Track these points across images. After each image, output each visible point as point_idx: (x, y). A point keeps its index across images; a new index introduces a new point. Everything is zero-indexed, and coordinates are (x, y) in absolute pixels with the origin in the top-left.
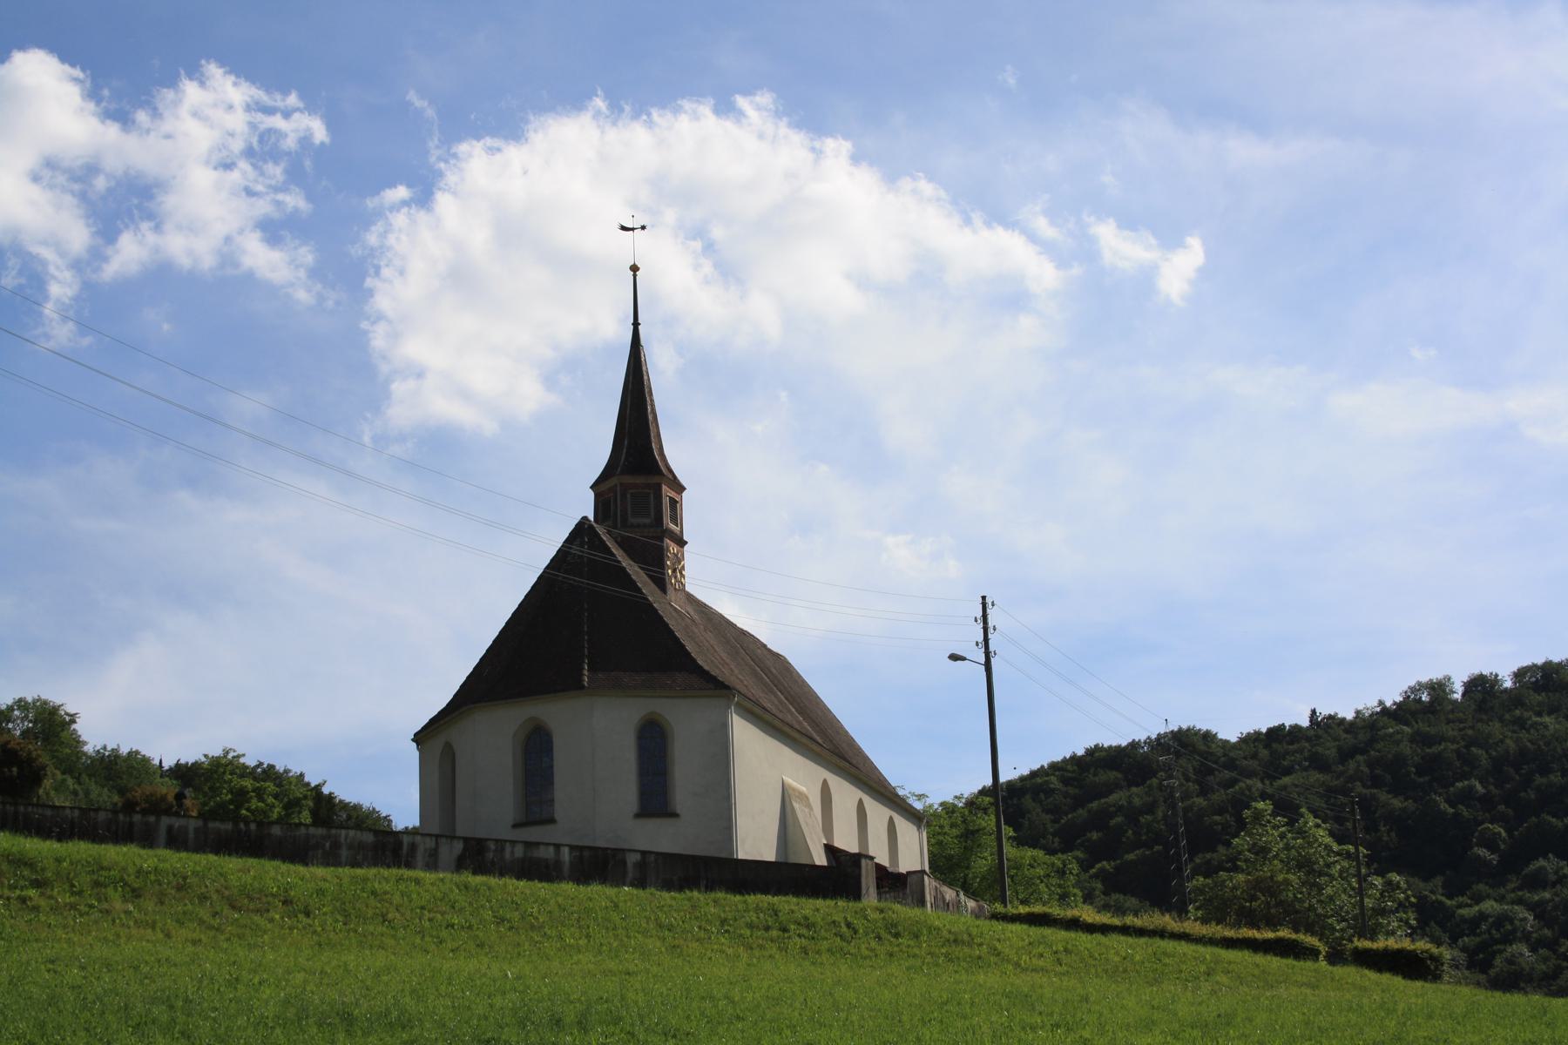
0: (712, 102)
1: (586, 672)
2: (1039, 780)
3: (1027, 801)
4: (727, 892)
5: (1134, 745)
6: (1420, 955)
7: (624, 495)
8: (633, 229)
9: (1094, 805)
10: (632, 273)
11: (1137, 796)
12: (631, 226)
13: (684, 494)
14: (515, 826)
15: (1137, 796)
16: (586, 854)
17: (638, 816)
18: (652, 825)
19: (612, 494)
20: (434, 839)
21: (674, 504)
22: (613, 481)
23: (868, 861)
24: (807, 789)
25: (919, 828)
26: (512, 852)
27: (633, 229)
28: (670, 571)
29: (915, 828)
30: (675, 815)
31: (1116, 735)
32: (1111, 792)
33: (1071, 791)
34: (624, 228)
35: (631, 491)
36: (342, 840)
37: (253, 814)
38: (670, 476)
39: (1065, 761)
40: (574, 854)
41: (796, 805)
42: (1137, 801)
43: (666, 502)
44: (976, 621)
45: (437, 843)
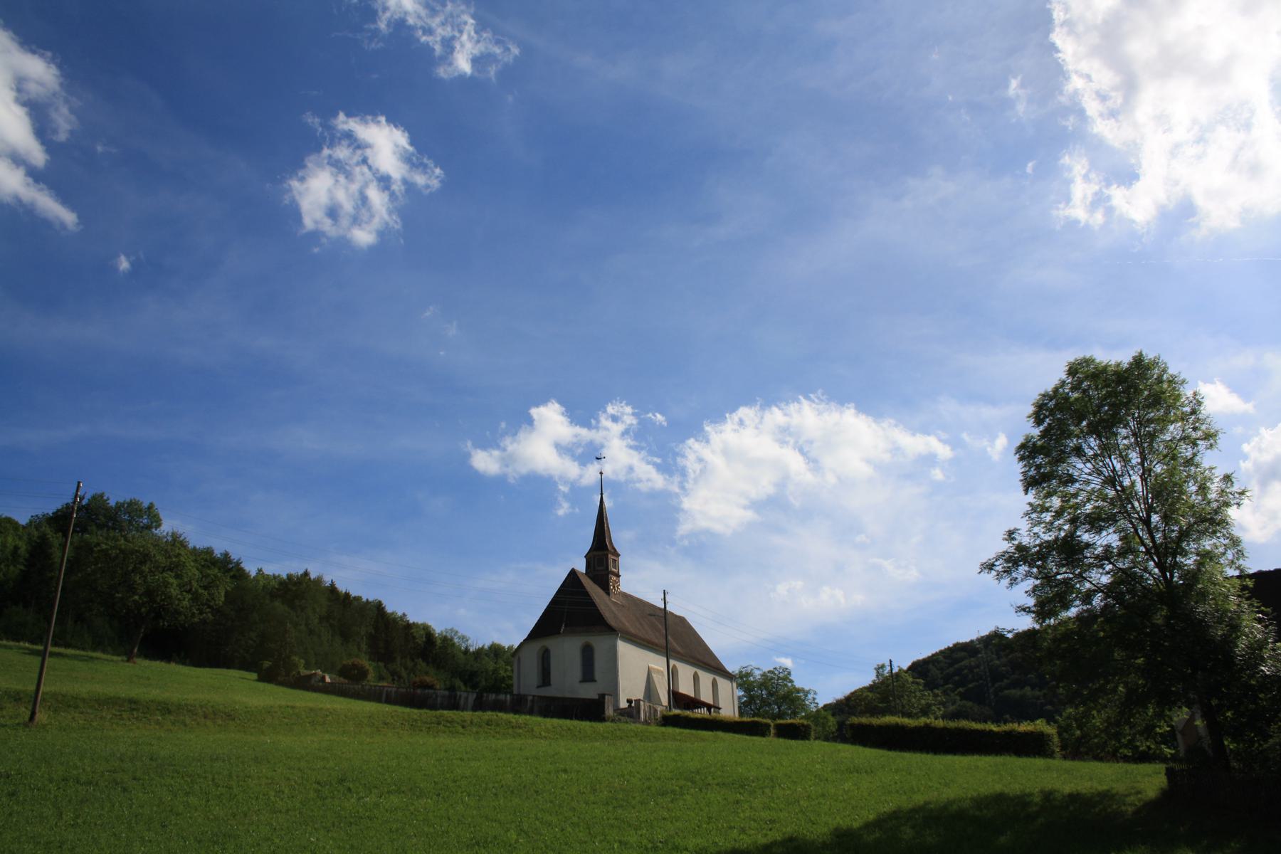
2: (934, 657)
3: (931, 666)
5: (972, 641)
9: (956, 666)
11: (973, 661)
14: (538, 687)
15: (973, 661)
16: (536, 698)
17: (580, 682)
18: (587, 685)
21: (614, 561)
23: (610, 697)
25: (731, 682)
30: (595, 681)
31: (965, 638)
32: (963, 660)
33: (947, 661)
38: (613, 551)
39: (945, 649)
42: (973, 663)
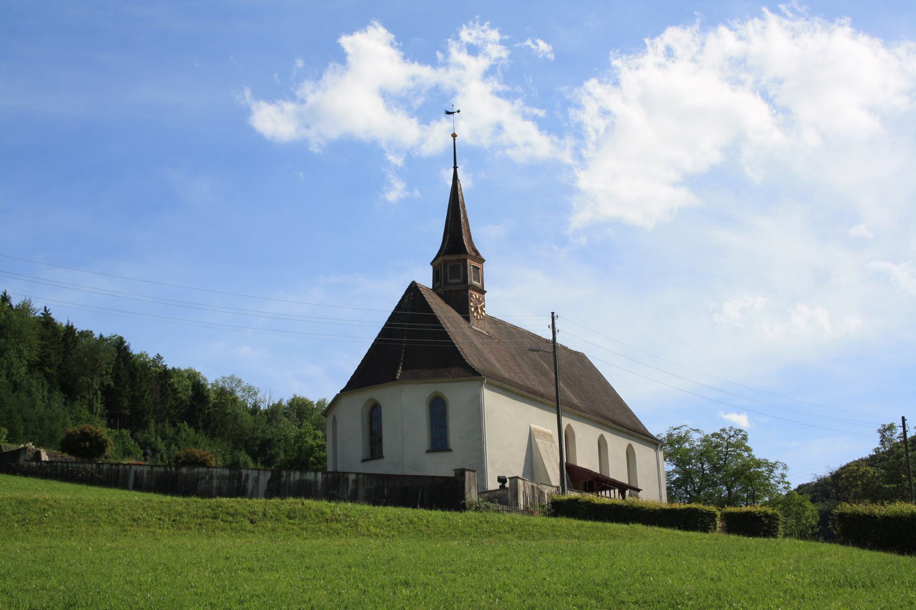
0: (849, 19)
1: (400, 371)
4: (172, 496)
6: (758, 515)
7: (445, 267)
13: (484, 264)
14: (363, 461)
20: (257, 471)
22: (440, 259)
25: (656, 450)
26: (294, 477)
28: (473, 309)
29: (652, 450)
30: (450, 450)
35: (449, 264)
36: (214, 474)
40: (323, 476)
41: (537, 440)
43: (470, 270)
44: (549, 327)
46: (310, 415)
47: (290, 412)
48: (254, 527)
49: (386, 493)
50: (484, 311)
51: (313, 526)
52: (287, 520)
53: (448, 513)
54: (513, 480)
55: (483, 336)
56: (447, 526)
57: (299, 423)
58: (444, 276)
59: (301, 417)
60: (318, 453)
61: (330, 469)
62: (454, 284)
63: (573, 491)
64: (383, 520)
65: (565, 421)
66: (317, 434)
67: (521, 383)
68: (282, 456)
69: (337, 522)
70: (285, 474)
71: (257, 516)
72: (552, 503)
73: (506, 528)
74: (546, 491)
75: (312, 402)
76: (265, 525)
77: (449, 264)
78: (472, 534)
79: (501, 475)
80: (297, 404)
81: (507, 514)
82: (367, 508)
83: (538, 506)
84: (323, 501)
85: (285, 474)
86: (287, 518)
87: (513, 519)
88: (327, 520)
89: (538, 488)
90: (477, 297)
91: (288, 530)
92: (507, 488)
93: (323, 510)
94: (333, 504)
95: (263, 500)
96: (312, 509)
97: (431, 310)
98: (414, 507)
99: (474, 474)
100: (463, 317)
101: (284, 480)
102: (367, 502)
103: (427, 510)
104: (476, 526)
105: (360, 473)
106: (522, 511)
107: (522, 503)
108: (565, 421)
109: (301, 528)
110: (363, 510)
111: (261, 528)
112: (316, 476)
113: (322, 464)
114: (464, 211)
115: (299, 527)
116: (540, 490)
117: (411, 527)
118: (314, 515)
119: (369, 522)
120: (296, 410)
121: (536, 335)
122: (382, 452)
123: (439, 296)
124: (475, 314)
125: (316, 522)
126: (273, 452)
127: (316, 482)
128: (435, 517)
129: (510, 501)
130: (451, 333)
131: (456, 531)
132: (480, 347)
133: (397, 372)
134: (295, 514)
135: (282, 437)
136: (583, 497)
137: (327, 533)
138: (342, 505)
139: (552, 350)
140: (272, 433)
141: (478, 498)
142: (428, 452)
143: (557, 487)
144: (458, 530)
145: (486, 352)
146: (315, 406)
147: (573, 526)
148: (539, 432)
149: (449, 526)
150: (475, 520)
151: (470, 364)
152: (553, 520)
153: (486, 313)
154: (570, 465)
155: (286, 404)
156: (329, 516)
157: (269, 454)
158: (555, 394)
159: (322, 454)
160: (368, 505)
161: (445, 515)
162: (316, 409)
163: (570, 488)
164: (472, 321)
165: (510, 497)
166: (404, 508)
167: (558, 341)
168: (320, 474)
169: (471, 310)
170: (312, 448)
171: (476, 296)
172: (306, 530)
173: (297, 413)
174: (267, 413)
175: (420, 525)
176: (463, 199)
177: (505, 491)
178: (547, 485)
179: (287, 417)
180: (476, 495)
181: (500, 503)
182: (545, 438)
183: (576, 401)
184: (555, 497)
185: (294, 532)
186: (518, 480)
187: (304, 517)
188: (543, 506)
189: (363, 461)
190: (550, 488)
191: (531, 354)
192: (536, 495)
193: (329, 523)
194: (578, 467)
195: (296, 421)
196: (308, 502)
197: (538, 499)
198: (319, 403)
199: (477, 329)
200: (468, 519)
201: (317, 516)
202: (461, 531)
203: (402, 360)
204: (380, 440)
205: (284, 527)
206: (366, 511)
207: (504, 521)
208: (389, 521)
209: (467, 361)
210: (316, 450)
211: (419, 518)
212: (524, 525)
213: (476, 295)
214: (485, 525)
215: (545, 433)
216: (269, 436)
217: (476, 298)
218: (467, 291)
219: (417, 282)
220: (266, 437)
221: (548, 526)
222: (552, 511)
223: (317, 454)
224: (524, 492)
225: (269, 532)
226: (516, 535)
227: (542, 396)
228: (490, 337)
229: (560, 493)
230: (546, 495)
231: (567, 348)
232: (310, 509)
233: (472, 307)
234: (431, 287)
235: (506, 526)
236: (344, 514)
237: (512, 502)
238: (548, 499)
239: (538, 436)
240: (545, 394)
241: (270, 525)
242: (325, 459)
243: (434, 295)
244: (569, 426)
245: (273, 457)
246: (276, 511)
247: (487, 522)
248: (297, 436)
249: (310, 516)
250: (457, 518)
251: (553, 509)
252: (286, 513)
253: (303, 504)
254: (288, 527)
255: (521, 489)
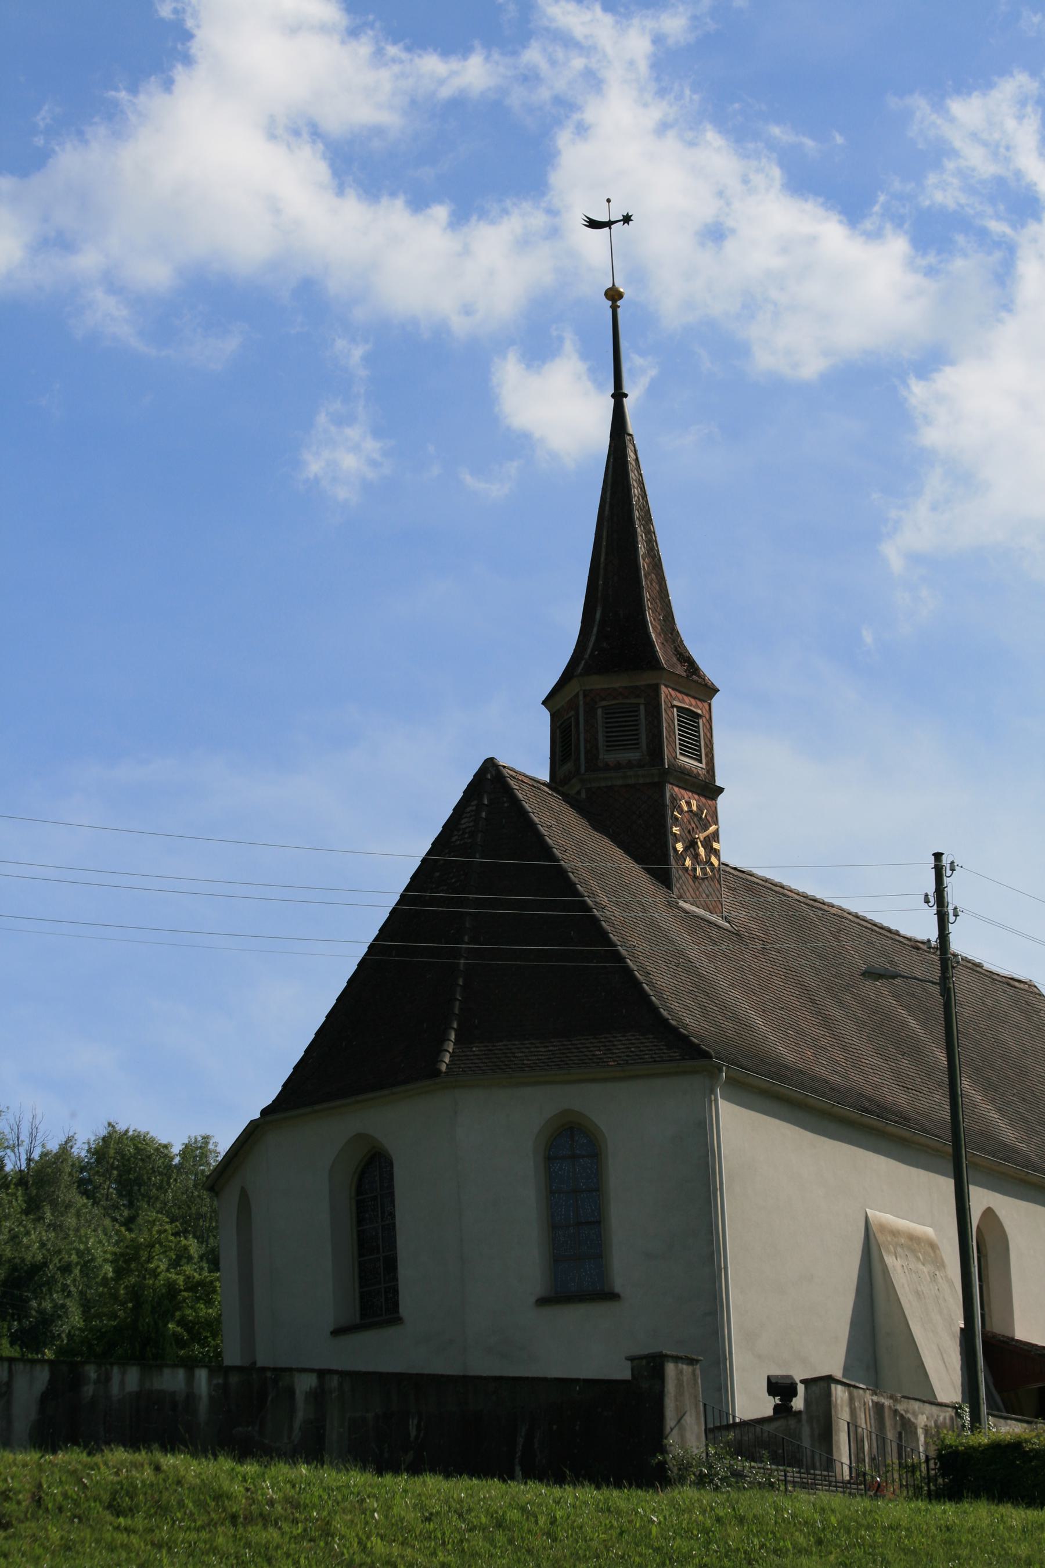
8: (609, 224)
10: (610, 303)
12: (604, 219)
13: (716, 701)
19: (572, 713)
20: (6, 1365)
23: (686, 1368)
24: (935, 1231)
26: (122, 1383)
27: (609, 224)
28: (680, 847)
30: (613, 1296)
34: (593, 224)
35: (604, 703)
37: (189, 1331)
40: (215, 1382)
41: (890, 1260)
43: (670, 719)
44: (927, 901)
45: (10, 1371)
46: (160, 1188)
47: (98, 1180)
48: (6, 1538)
49: (413, 1433)
50: (717, 853)
51: (193, 1536)
52: (109, 1517)
53: (616, 1493)
54: (815, 1389)
55: (714, 933)
56: (614, 1533)
57: (126, 1213)
58: (586, 740)
59: (130, 1194)
60: (192, 1308)
61: (232, 1357)
62: (618, 766)
63: (1006, 1418)
64: (412, 1516)
65: (980, 1199)
66: (186, 1248)
67: (836, 1079)
68: (75, 1318)
69: (265, 1527)
70: (93, 1375)
71: (14, 1507)
72: (940, 1457)
73: (801, 1540)
74: (921, 1421)
75: (166, 1146)
76: (42, 1534)
77: (604, 703)
78: (694, 1557)
79: (777, 1371)
80: (120, 1152)
81: (803, 1495)
82: (358, 1479)
83: (896, 1467)
84: (221, 1459)
85: (93, 1375)
86: (107, 1512)
87: (823, 1510)
88: (234, 1518)
89: (896, 1411)
90: (694, 808)
91: (111, 1548)
92: (800, 1412)
93: (220, 1487)
94: (250, 1468)
95: (32, 1457)
96: (186, 1486)
97: (547, 852)
98: (506, 1475)
99: (694, 1373)
100: (648, 871)
101: (91, 1393)
102: (360, 1464)
103: (548, 1485)
104: (706, 1531)
105: (330, 1372)
106: (846, 1484)
107: (846, 1460)
108: (980, 1199)
109: (153, 1544)
110: (348, 1486)
111: (28, 1540)
112: (190, 1379)
113: (204, 1343)
114: (650, 533)
115: (148, 1538)
116: (902, 1416)
117: (500, 1537)
118: (194, 1502)
119: (367, 1523)
120: (115, 1172)
121: (882, 928)
122: (396, 1305)
123: (572, 806)
124: (688, 863)
125: (199, 1523)
126: (47, 1305)
127: (191, 1397)
128: (574, 1506)
129: (809, 1453)
130: (613, 925)
131: (642, 1549)
132: (705, 965)
133: (440, 1050)
134: (131, 1498)
135: (74, 1258)
136: (1038, 1436)
137: (237, 1558)
138: (282, 1470)
139: (936, 975)
140: (43, 1245)
141: (707, 1445)
142: (543, 1302)
143: (956, 1408)
144: (650, 1546)
145: (724, 984)
146: (177, 1160)
147: (1012, 1527)
148: (895, 1233)
149: (621, 1533)
150: (703, 1512)
151: (673, 1023)
152: (947, 1511)
153: (723, 859)
154: (995, 1336)
155: (83, 1154)
156: (237, 1507)
157: (34, 1313)
158: (947, 1116)
159: (204, 1311)
160: (364, 1469)
161: (606, 1501)
162: (179, 1167)
163: (994, 1410)
164: (676, 886)
165: (806, 1443)
166: (475, 1481)
167: (958, 945)
168: (202, 1375)
169: (675, 849)
170: (172, 1289)
171: (689, 804)
172: (169, 1549)
173: (118, 1181)
174: (26, 1183)
175: (529, 1531)
176: (644, 495)
177: (792, 1422)
178: (924, 1402)
179: (86, 1193)
180: (698, 1438)
181: (776, 1460)
182: (913, 1251)
183: (1009, 1134)
184: (950, 1439)
185: (133, 1555)
186: (833, 1386)
187: (162, 1509)
188: (913, 1468)
189: (336, 1332)
190: (934, 1409)
191: (870, 989)
192: (890, 1435)
193: (241, 1530)
194: (1018, 1341)
195: (116, 1207)
196: (170, 1461)
197: (895, 1446)
198: (188, 1151)
199: (694, 908)
200: (679, 1512)
201: (201, 1505)
202: (657, 1550)
203: (457, 1011)
204: (391, 1265)
205: (98, 1541)
206: (356, 1490)
207: (794, 1516)
208: (428, 1519)
209: (665, 1013)
210: (184, 1300)
211: (523, 1509)
212: (858, 1529)
213: (689, 801)
214: (734, 1531)
215: (913, 1238)
216: (34, 1253)
217: (691, 811)
218: (660, 788)
219: (502, 761)
220: (23, 1260)
221: (934, 1530)
222: (940, 1481)
223: (188, 1312)
224: (853, 1426)
225: (53, 1553)
226: (832, 1558)
227: (903, 1119)
228: (737, 934)
229: (963, 1426)
230: (920, 1432)
231: (980, 965)
232: (179, 1483)
233: (677, 840)
234: (545, 777)
235: (801, 1531)
236: (287, 1500)
237: (813, 1457)
238: (926, 1444)
239: (891, 1248)
240: (913, 1115)
241: (55, 1533)
242: (213, 1326)
243: (557, 803)
244: (989, 1213)
245: (46, 1320)
246: (73, 1490)
247: (741, 1520)
248: (122, 1255)
249: (181, 1504)
250: (645, 1511)
251: (943, 1476)
252: (106, 1497)
253: (157, 1468)
254: (113, 1539)
255: (842, 1416)
